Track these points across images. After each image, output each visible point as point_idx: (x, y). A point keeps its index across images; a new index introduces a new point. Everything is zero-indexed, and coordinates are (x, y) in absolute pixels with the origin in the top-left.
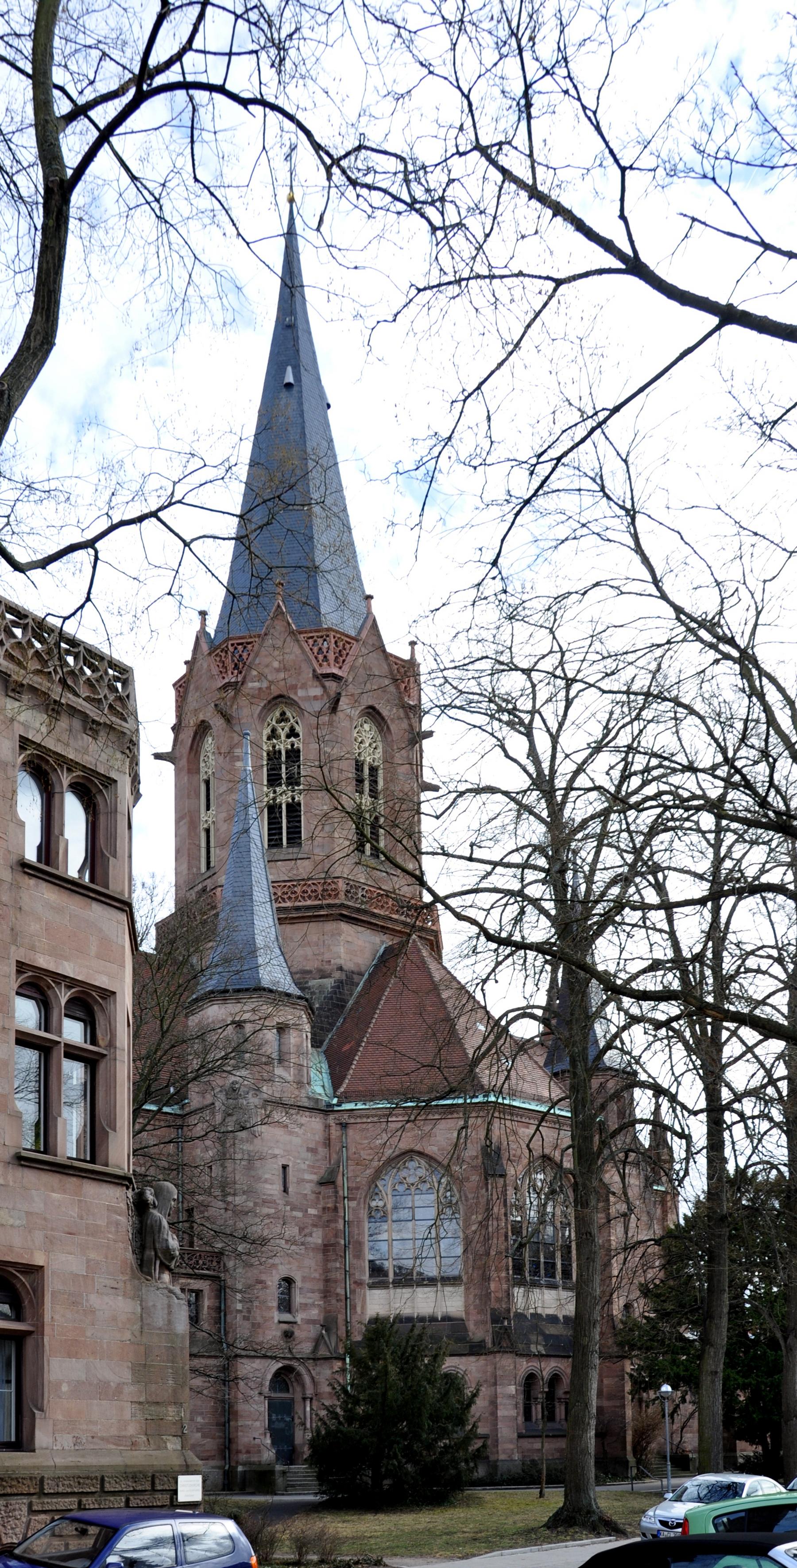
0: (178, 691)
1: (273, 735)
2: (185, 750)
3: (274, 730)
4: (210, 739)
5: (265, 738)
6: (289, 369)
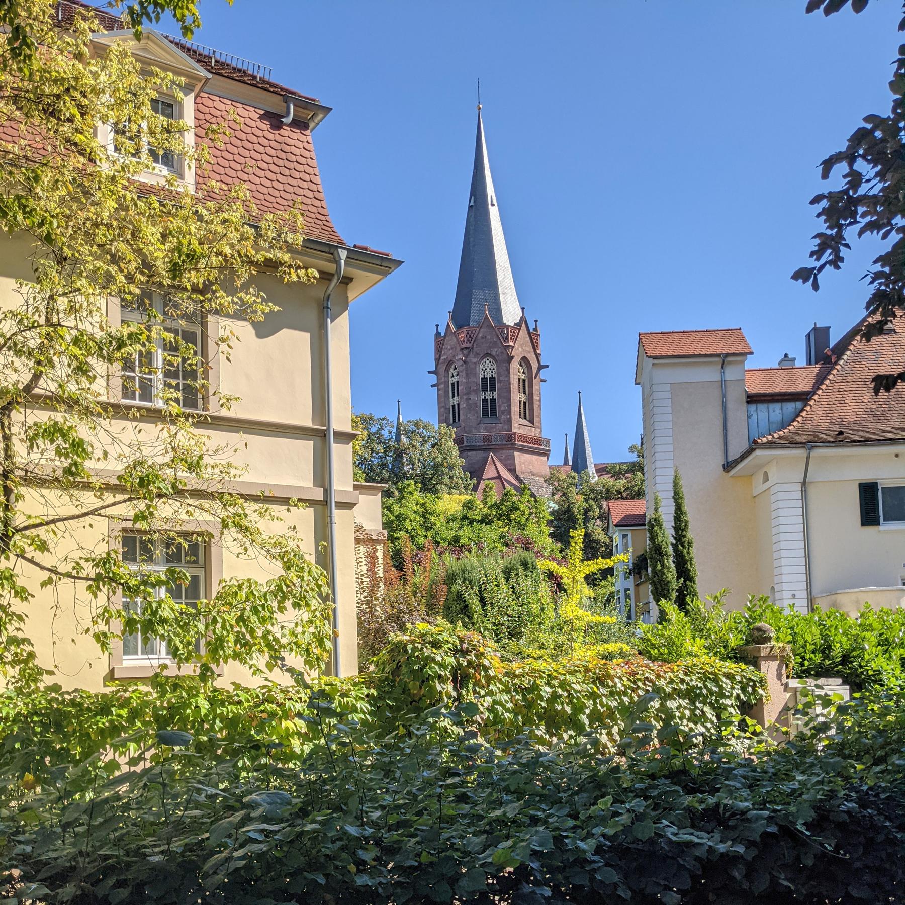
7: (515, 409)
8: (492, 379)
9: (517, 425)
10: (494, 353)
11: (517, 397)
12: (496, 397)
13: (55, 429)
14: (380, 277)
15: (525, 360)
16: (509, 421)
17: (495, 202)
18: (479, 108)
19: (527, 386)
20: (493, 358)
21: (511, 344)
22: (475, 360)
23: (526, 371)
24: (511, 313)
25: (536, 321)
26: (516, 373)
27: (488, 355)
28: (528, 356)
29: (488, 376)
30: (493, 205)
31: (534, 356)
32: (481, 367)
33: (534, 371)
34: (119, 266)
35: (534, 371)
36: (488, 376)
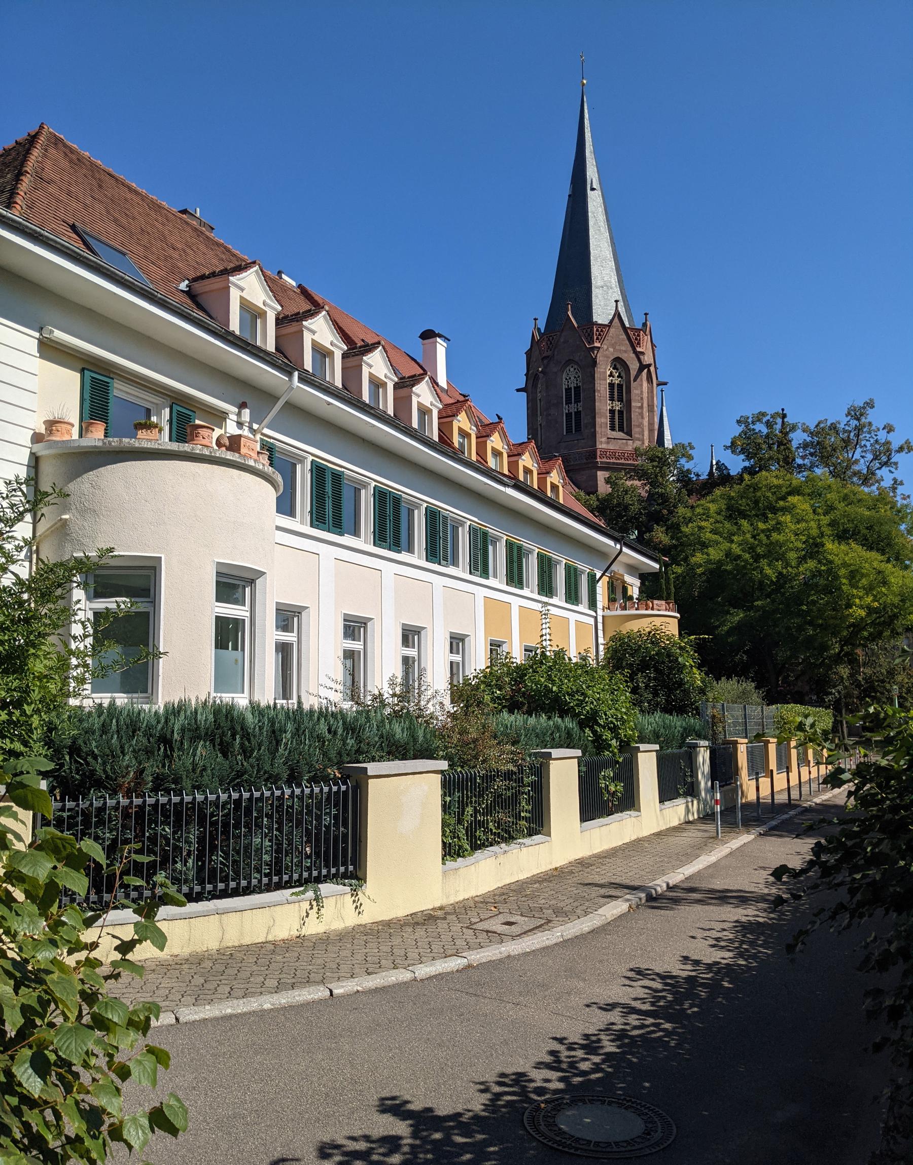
2: (530, 386)
4: (572, 369)
7: (603, 420)
8: (577, 388)
9: (604, 440)
10: (577, 359)
11: (604, 405)
12: (580, 409)
13: (71, 895)
14: (38, 355)
15: (619, 363)
16: (594, 435)
17: (596, 185)
18: (583, 84)
19: (621, 392)
20: (577, 363)
21: (597, 344)
22: (555, 370)
23: (623, 374)
24: (602, 312)
25: (646, 314)
26: (605, 375)
27: (569, 362)
28: (624, 356)
29: (572, 386)
30: (593, 189)
31: (633, 356)
32: (564, 376)
33: (633, 373)
34: (57, 1055)
35: (633, 373)
36: (572, 386)
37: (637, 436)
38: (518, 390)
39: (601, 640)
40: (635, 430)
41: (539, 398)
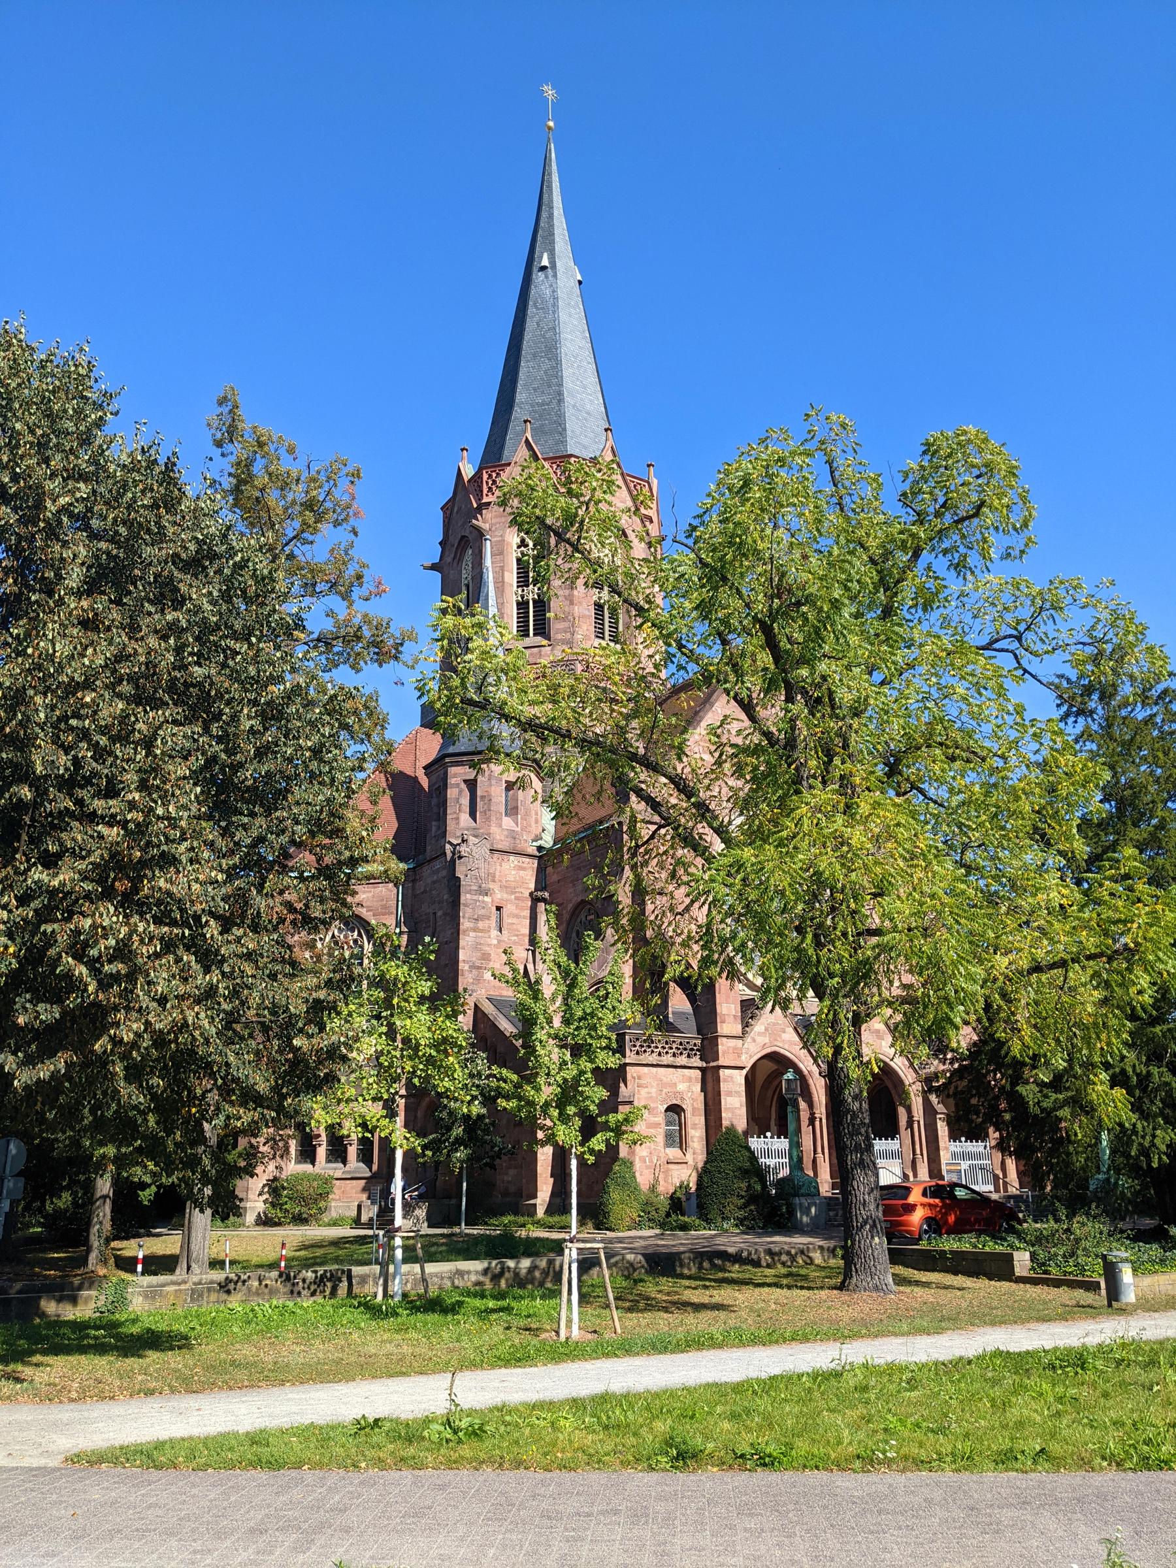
0: (445, 513)
1: (523, 544)
2: (449, 559)
3: (523, 541)
5: (515, 547)
6: (545, 256)
37: (559, 636)
38: (426, 568)
39: (653, 1059)
40: (556, 627)
41: (464, 582)
